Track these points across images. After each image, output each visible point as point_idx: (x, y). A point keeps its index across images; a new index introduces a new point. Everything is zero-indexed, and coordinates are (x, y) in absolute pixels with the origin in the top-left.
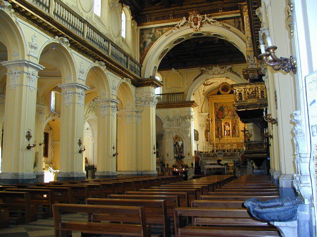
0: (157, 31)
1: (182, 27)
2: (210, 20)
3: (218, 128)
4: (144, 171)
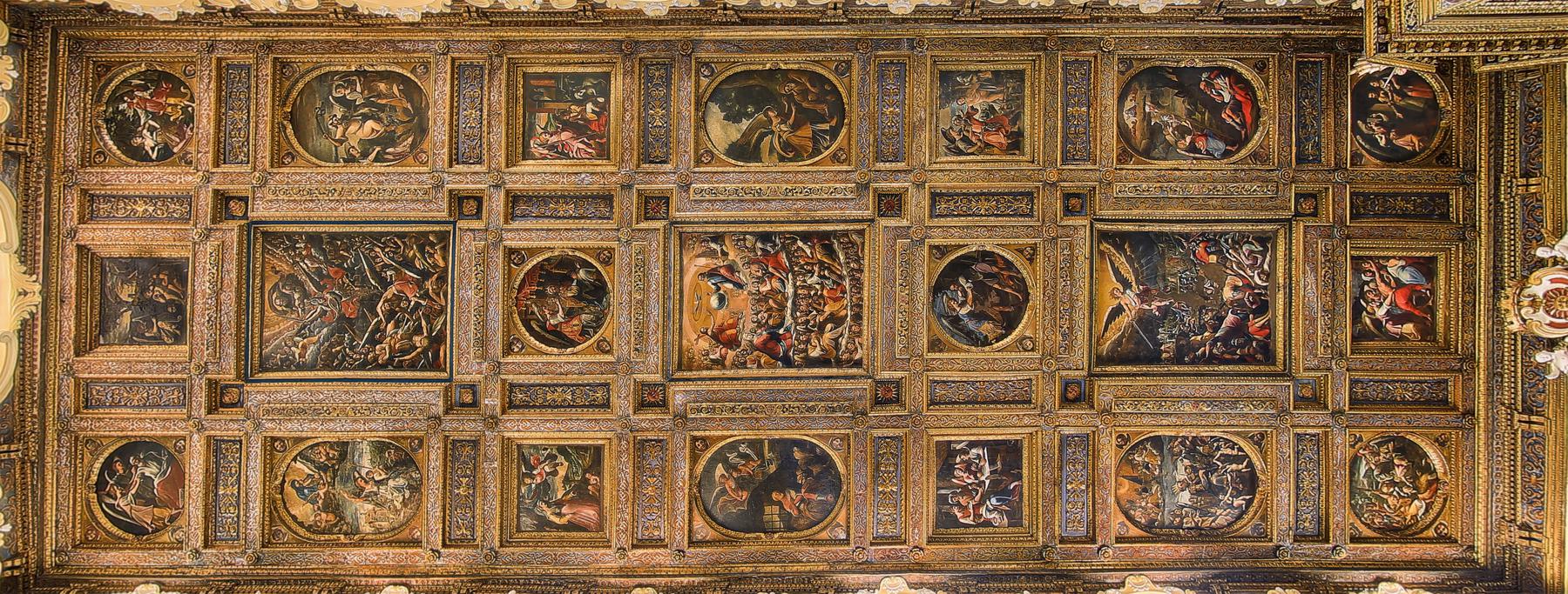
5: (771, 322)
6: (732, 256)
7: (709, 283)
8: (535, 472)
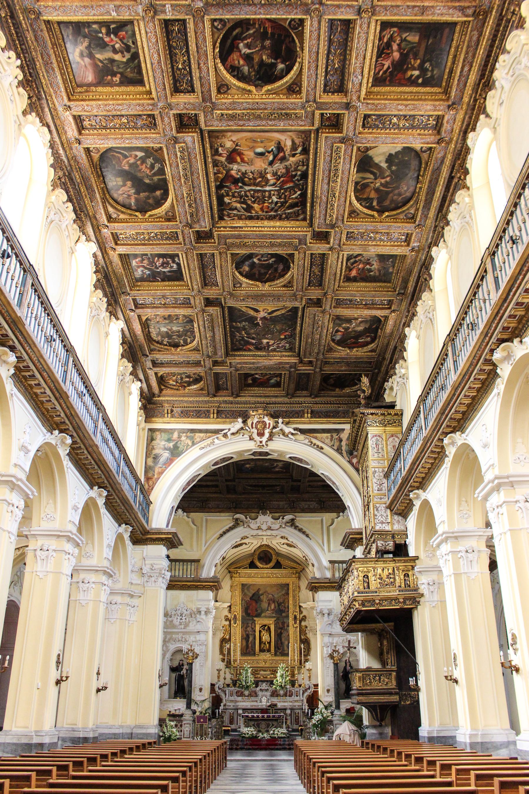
0: (183, 438)
1: (233, 436)
2: (287, 430)
3: (248, 636)
4: (136, 727)
5: (246, 179)
6: (292, 159)
7: (273, 147)
8: (112, 36)
